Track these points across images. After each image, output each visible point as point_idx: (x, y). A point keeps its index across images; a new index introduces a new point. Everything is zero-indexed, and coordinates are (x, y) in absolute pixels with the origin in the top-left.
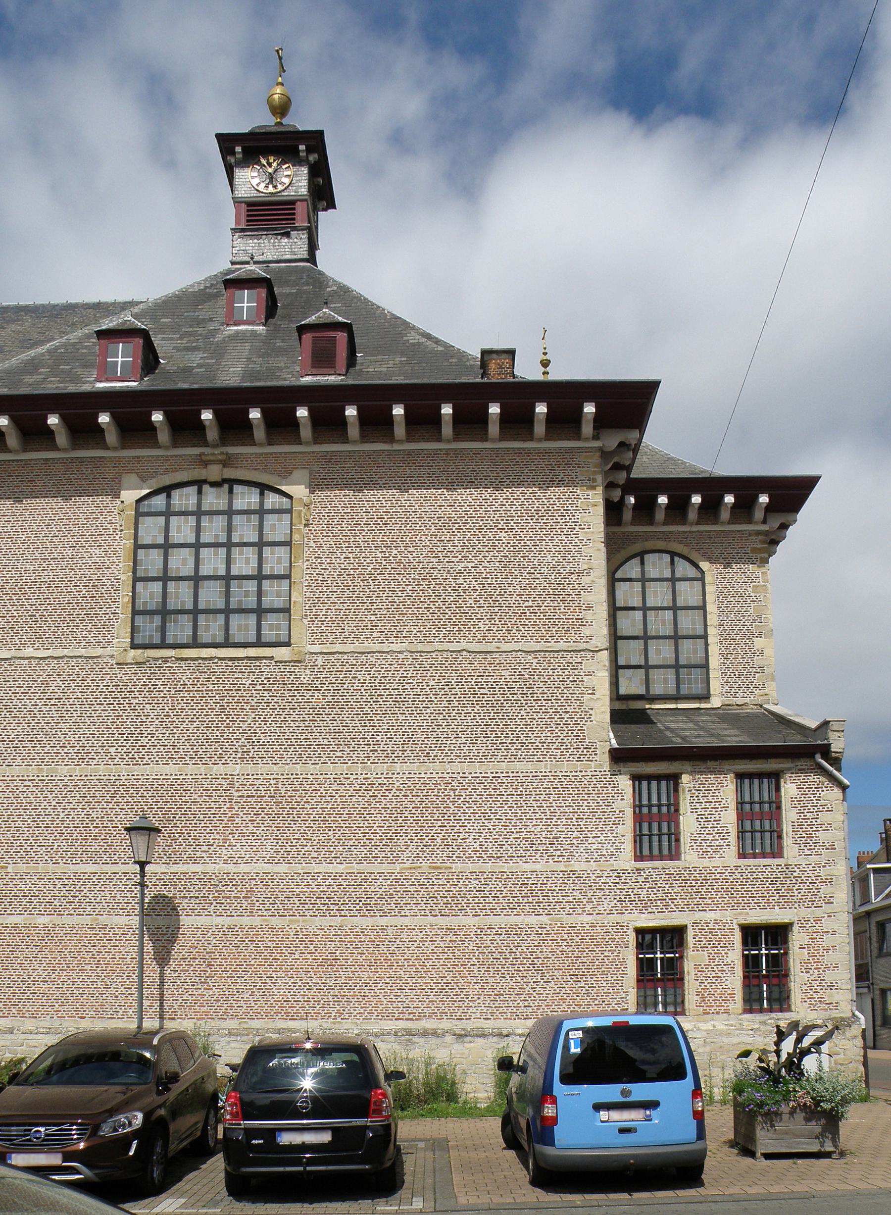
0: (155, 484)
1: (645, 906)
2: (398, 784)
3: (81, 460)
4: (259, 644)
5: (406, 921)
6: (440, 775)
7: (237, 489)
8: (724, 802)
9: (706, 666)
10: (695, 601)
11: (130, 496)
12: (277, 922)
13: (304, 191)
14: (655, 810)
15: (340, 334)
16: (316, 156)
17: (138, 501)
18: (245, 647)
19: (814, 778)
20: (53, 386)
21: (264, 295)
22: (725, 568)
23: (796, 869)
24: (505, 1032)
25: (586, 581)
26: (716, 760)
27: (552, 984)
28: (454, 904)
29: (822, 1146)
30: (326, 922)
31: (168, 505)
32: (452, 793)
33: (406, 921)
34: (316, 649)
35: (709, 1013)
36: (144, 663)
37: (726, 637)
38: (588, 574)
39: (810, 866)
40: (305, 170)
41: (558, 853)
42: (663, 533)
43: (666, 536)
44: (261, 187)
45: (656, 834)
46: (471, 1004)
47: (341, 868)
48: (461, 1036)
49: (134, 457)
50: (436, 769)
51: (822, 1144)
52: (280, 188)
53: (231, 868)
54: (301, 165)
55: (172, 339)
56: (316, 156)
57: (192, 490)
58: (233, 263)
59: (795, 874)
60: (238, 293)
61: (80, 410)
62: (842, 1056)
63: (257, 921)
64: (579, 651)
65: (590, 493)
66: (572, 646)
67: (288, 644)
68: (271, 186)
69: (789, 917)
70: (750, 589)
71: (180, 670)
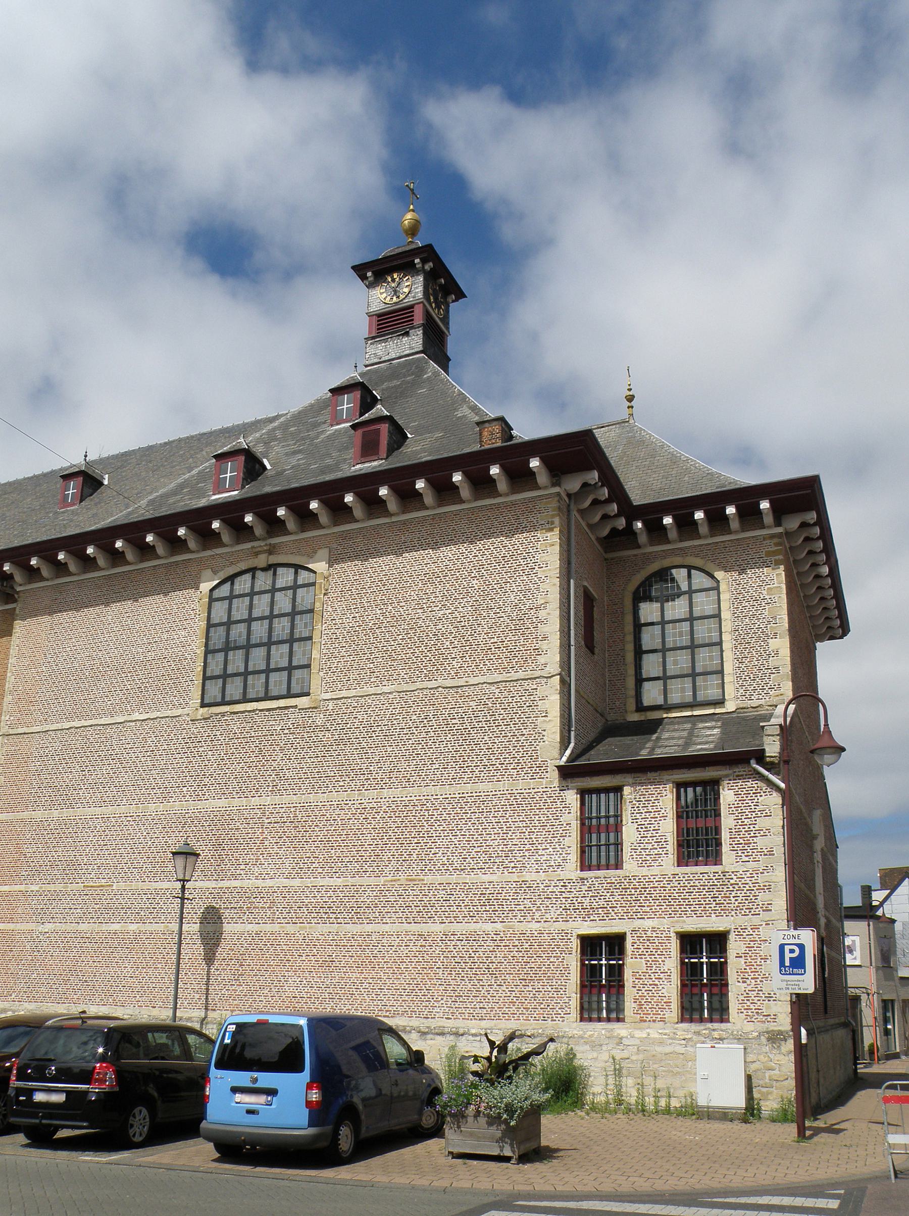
0: (223, 575)
1: (587, 914)
2: (385, 807)
3: (176, 563)
4: (289, 695)
5: (386, 928)
6: (418, 798)
7: (280, 571)
8: (663, 811)
9: (721, 672)
10: (709, 609)
11: (206, 587)
12: (290, 928)
13: (420, 295)
14: (603, 821)
15: (383, 425)
16: (431, 264)
17: (212, 590)
18: (278, 699)
19: (752, 784)
20: (180, 507)
21: (359, 396)
22: (740, 574)
23: (733, 876)
24: (461, 1031)
25: (542, 614)
26: (656, 771)
27: (504, 988)
28: (425, 914)
29: (502, 1151)
30: (326, 928)
31: (232, 590)
32: (426, 814)
33: (386, 928)
34: (328, 696)
35: (645, 1021)
36: (209, 718)
37: (740, 642)
38: (545, 608)
39: (748, 873)
40: (421, 278)
41: (512, 865)
42: (681, 549)
43: (683, 552)
44: (388, 300)
45: (600, 845)
46: (436, 1004)
47: (339, 882)
48: (424, 1033)
49: (211, 556)
50: (414, 793)
51: (502, 1149)
52: (402, 297)
53: (260, 883)
54: (418, 275)
55: (289, 445)
56: (431, 264)
57: (248, 577)
58: (366, 366)
59: (732, 881)
60: (340, 398)
61: (197, 519)
62: (777, 1072)
63: (276, 927)
64: (535, 678)
65: (549, 534)
66: (529, 674)
67: (308, 694)
68: (395, 298)
69: (726, 925)
70: (765, 592)
71: (237, 720)
